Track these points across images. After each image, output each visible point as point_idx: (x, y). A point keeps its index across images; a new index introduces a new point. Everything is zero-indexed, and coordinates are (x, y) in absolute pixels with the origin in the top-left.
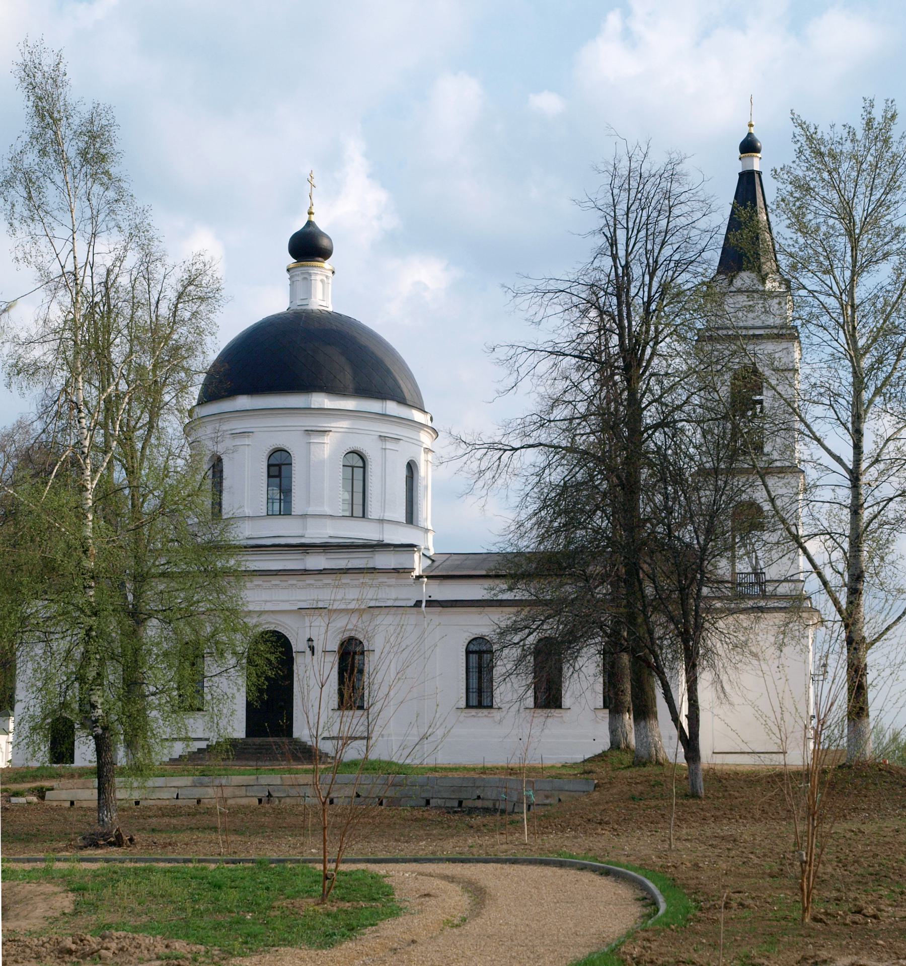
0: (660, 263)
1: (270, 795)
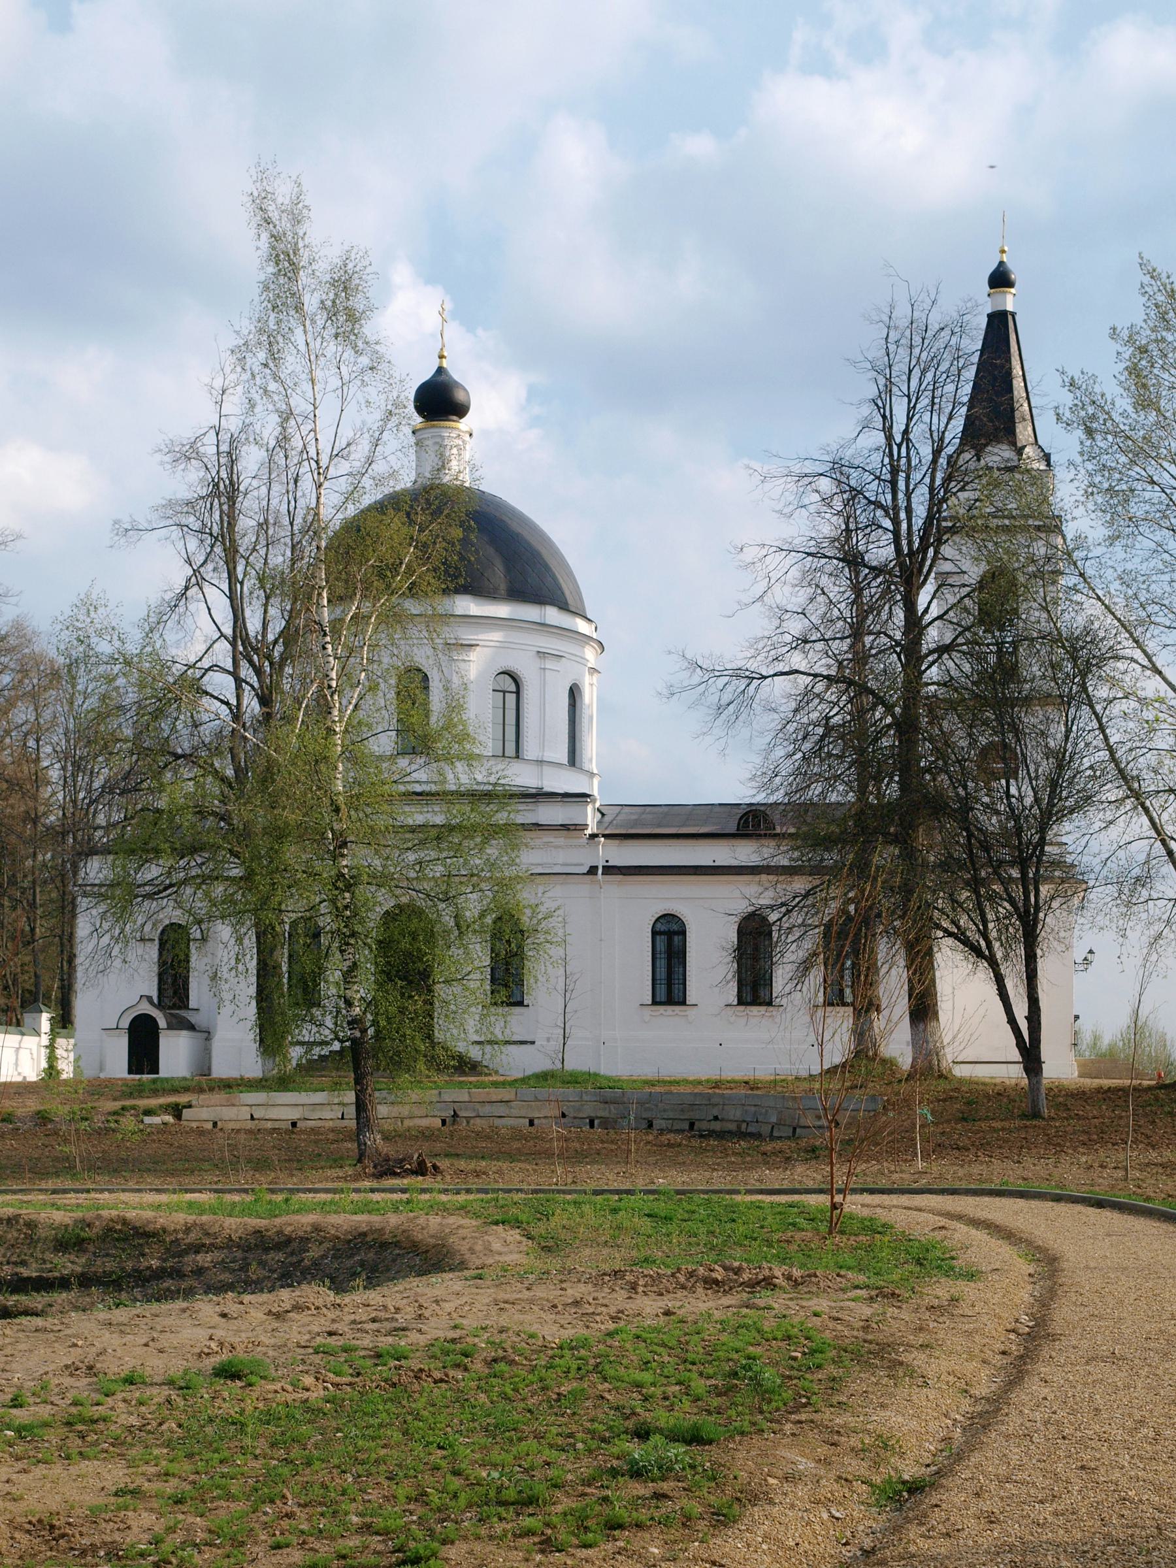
0: (946, 441)
1: (455, 1115)
